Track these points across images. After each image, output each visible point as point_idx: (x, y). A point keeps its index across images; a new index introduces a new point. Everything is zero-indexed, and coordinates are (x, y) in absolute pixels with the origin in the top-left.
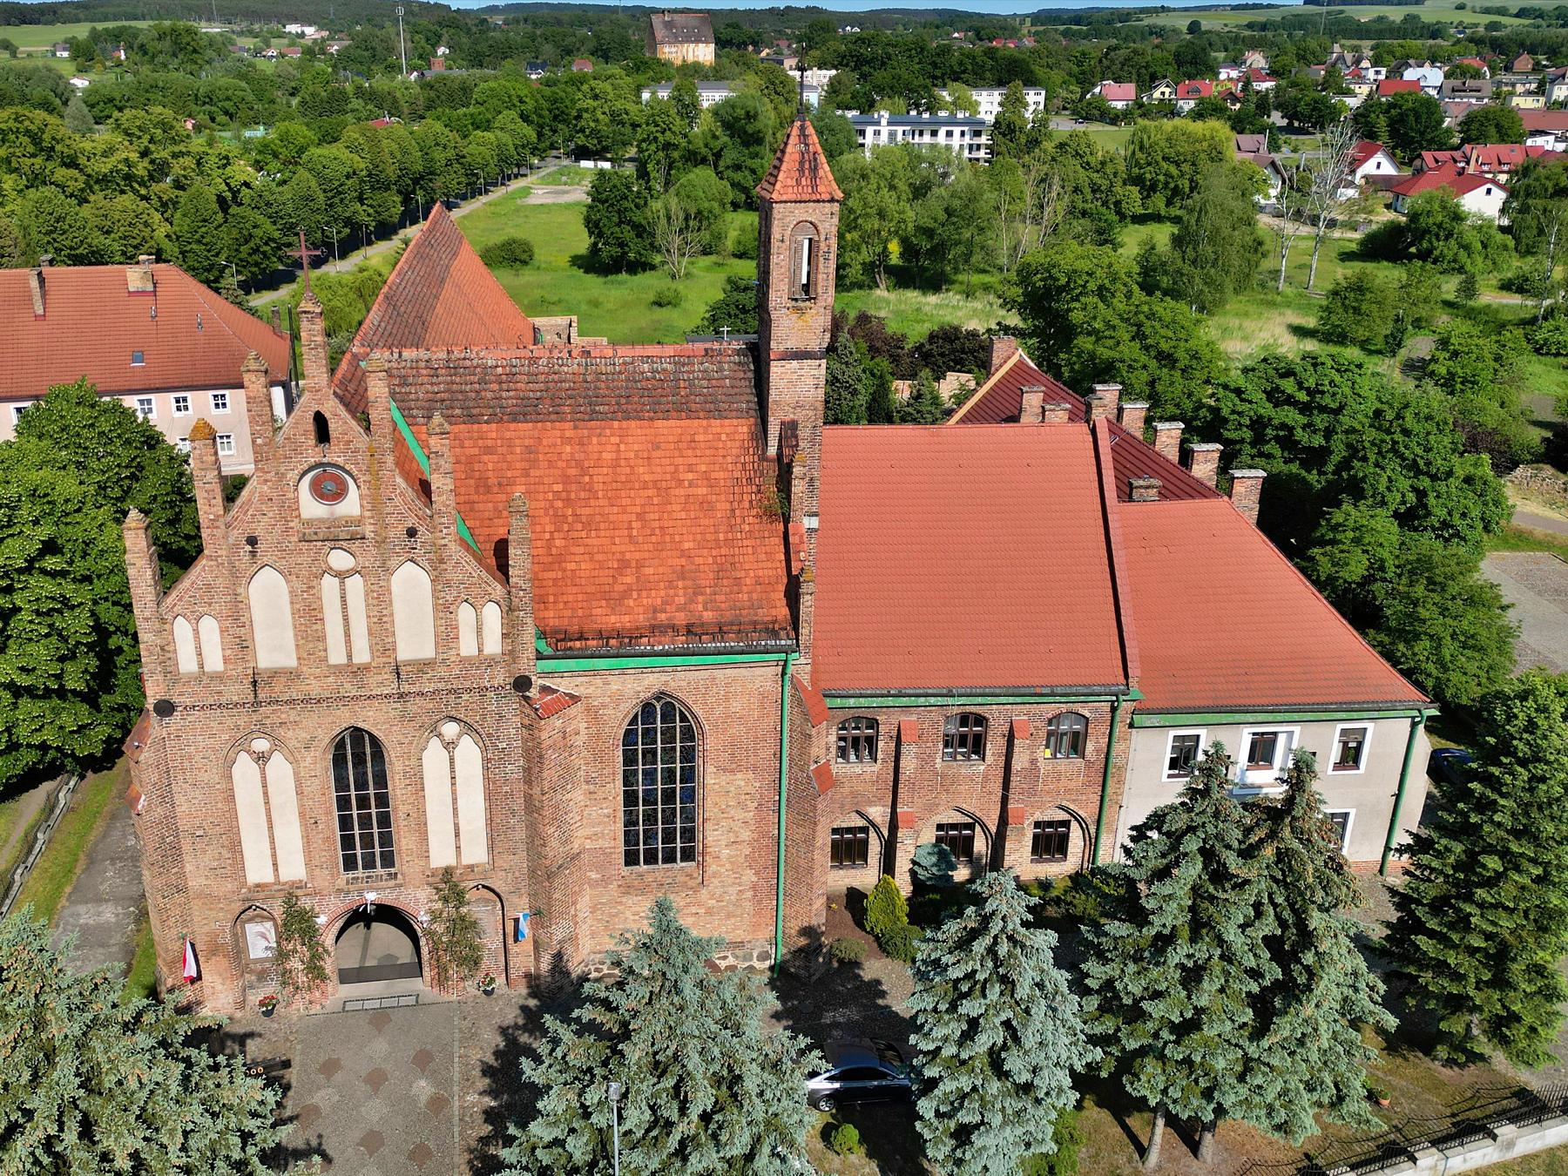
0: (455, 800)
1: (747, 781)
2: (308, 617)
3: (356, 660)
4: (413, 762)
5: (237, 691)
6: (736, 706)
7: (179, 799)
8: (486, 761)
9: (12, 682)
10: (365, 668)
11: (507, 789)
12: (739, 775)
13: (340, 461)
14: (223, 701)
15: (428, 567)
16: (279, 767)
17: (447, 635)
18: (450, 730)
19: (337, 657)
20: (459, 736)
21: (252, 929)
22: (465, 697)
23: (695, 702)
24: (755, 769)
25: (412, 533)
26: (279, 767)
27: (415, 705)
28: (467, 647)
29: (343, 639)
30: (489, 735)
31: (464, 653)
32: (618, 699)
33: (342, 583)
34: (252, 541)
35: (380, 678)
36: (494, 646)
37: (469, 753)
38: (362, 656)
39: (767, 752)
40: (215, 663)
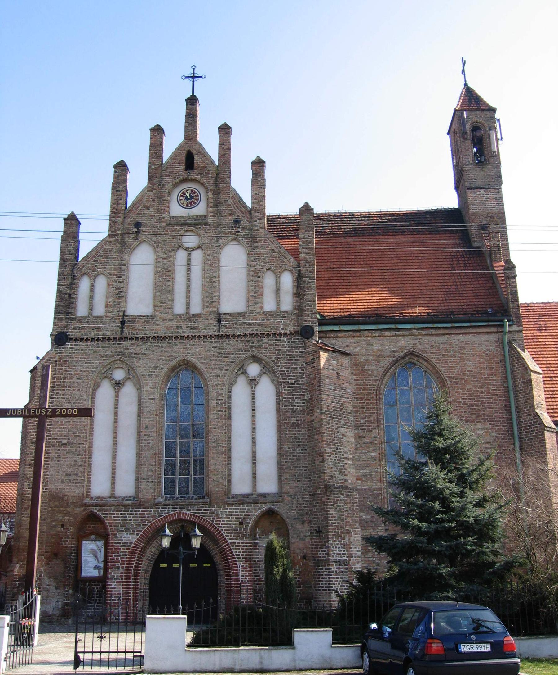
1: (486, 430)
2: (164, 276)
4: (225, 391)
5: (110, 329)
6: (470, 365)
8: (278, 394)
11: (293, 420)
12: (479, 426)
13: (198, 178)
16: (129, 392)
17: (255, 293)
18: (254, 369)
19: (179, 308)
20: (260, 375)
23: (438, 361)
24: (490, 419)
25: (237, 221)
26: (129, 392)
27: (232, 345)
28: (269, 305)
29: (187, 298)
30: (282, 373)
32: (379, 356)
33: (189, 254)
34: (138, 225)
35: (207, 323)
36: (287, 304)
37: (266, 391)
38: (196, 309)
39: (499, 406)
40: (100, 310)
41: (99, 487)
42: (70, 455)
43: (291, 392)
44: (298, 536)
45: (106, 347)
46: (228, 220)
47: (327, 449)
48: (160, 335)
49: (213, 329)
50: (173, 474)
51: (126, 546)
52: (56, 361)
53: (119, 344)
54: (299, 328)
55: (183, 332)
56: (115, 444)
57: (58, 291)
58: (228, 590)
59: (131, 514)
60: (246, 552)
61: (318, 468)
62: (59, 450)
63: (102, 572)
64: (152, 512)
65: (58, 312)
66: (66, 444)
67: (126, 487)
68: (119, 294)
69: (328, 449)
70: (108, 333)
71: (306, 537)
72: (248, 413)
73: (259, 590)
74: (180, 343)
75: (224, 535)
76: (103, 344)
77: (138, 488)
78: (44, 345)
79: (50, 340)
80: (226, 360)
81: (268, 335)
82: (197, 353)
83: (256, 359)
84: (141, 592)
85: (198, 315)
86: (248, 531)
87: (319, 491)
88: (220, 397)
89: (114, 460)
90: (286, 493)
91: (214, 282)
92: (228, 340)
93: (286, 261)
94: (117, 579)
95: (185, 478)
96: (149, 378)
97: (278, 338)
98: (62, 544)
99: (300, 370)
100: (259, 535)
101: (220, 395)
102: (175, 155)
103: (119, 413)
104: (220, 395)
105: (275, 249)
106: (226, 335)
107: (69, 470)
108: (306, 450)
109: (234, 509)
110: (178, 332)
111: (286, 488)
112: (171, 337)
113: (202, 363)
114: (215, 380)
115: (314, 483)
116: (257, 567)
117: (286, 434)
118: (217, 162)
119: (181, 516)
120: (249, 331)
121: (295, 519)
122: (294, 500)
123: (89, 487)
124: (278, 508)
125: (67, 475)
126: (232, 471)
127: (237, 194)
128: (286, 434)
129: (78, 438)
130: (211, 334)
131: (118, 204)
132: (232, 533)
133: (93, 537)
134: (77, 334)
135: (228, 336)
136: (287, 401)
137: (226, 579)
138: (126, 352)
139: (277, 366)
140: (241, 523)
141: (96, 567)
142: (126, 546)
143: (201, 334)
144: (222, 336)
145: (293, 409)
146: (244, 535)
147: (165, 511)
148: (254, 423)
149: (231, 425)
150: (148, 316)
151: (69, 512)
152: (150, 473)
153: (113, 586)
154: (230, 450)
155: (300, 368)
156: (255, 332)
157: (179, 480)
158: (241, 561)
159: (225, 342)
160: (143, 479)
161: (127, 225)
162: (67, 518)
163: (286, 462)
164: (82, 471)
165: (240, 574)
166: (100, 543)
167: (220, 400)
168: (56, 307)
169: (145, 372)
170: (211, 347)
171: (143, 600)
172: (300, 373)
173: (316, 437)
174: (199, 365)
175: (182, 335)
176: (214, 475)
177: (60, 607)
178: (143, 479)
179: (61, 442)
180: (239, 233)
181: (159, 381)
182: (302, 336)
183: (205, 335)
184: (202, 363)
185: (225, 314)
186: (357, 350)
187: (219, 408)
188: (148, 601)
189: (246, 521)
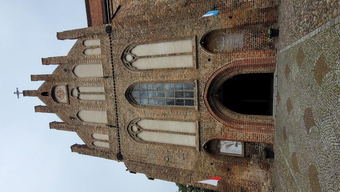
0: (158, 56)
3: (108, 139)
4: (139, 73)
7: (152, 162)
9: (111, 121)
10: (106, 90)
11: (151, 33)
14: (117, 137)
15: (74, 65)
16: (143, 124)
17: (94, 59)
18: (129, 58)
21: (224, 149)
22: (113, 52)
28: (98, 52)
31: (100, 53)
38: (102, 89)
41: (192, 141)
42: (174, 156)
43: (138, 35)
44: (217, 23)
45: (122, 135)
46: (65, 74)
47: (164, 9)
48: (115, 107)
49: (110, 80)
50: (183, 100)
51: (223, 129)
52: (129, 160)
53: (120, 128)
54: (108, 34)
55: (113, 96)
56: (167, 132)
57: (100, 157)
58: (251, 66)
59: (204, 125)
60: (227, 55)
61: (176, 13)
62: (171, 162)
63: (239, 143)
64: (203, 113)
65: (109, 158)
66: (168, 158)
67: (191, 127)
68: (99, 128)
69: (164, 8)
70: (116, 134)
71: (218, 18)
72: (151, 60)
73: (252, 47)
74: (118, 97)
75: (216, 70)
76: (121, 136)
77: (190, 121)
78: (122, 165)
79: (121, 162)
80: (124, 73)
81: (111, 51)
82: (122, 89)
83: (123, 57)
84: (252, 120)
85: (105, 88)
86: (214, 55)
87: (189, 11)
88: (142, 75)
89: (180, 132)
90: (191, 33)
91: (90, 81)
92: (115, 72)
93: (79, 44)
94: (244, 135)
95: (185, 94)
96: (134, 113)
97: (112, 46)
98: (222, 166)
99: (127, 32)
100: (217, 50)
101: (140, 75)
102: (43, 101)
103: (153, 129)
104: (140, 75)
105: (74, 51)
106: (113, 73)
107: (182, 157)
108: (167, 24)
109: (201, 65)
110: (113, 99)
111: (188, 34)
112: (116, 102)
113: (126, 86)
114: (134, 78)
115: (185, 15)
116: (237, 50)
117: (159, 37)
118: (44, 81)
119: (205, 96)
120: (110, 61)
121: (206, 26)
122: (195, 28)
123: (190, 147)
124: (200, 37)
125: (184, 159)
126: (180, 67)
127: (54, 71)
128: (159, 37)
129: (165, 152)
130: (113, 82)
131: (64, 127)
132: (215, 65)
133: (219, 146)
134: (117, 149)
135: (113, 72)
136: (142, 37)
137: (244, 68)
138: (123, 125)
139: (125, 45)
140: (209, 60)
141: (236, 146)
142: (223, 129)
143: (113, 86)
144: (113, 75)
145: (146, 34)
146: (217, 58)
147: (202, 105)
148: (154, 56)
149: (155, 69)
150: (107, 114)
151: (204, 160)
152: (182, 114)
153: (248, 138)
154: (168, 69)
155: (126, 32)
156: (111, 58)
157: (186, 97)
158: (232, 59)
159: (116, 74)
160: (185, 118)
161: (70, 122)
162: (207, 161)
163: (174, 35)
164: (182, 151)
165: (241, 59)
166: (221, 141)
167: (143, 76)
168: (107, 158)
169: (132, 116)
170: (119, 81)
171: (257, 119)
172: (128, 31)
173: (158, 17)
174: (127, 87)
175: (114, 96)
176: (182, 77)
177: (261, 171)
178: (185, 118)
179: (167, 161)
180: (70, 69)
181: (135, 108)
182: (111, 32)
183: (113, 84)
184: (126, 86)
185: (104, 75)
186: (118, 2)
187: (147, 76)
188: (257, 116)
189: (208, 57)
